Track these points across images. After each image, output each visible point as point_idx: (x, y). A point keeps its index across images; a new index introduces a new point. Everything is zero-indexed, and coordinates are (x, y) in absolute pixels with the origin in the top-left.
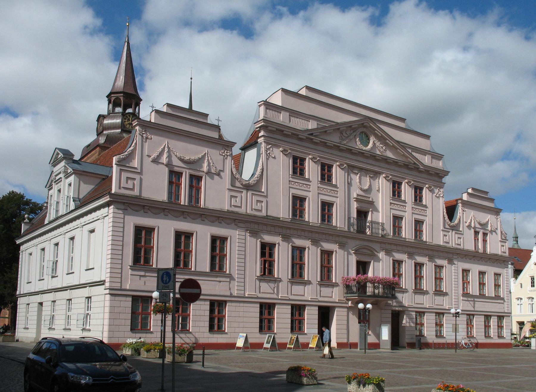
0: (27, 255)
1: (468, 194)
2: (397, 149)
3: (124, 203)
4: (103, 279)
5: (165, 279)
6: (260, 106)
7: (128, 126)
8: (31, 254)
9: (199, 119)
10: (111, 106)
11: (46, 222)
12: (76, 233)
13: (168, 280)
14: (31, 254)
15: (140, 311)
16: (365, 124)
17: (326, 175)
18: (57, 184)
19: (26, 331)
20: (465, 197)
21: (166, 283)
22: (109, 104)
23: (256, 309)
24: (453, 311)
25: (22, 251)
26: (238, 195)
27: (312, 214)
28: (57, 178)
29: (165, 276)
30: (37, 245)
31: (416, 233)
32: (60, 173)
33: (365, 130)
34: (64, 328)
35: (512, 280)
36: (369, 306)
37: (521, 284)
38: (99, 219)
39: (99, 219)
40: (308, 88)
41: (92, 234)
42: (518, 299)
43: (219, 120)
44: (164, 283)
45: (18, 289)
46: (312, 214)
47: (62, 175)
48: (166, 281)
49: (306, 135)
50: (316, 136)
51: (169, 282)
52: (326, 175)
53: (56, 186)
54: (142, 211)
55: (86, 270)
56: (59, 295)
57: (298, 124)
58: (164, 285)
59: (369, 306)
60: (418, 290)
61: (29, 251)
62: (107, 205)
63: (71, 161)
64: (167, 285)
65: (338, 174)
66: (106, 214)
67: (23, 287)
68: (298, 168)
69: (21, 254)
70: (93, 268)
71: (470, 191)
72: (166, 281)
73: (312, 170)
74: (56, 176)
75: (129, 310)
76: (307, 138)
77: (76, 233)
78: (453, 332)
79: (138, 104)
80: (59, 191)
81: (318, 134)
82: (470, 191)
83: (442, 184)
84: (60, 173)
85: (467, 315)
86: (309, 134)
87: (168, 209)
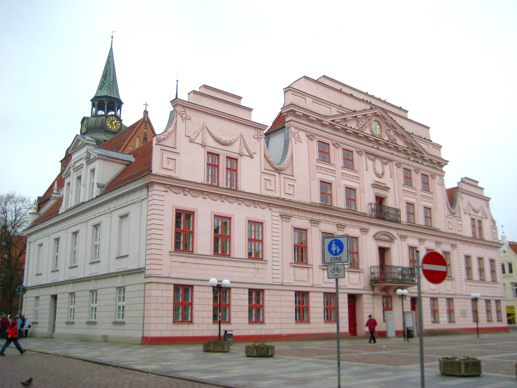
0: (37, 247)
2: (405, 137)
3: (165, 184)
4: (142, 266)
5: (333, 249)
8: (41, 245)
9: (233, 100)
10: (94, 109)
13: (338, 250)
14: (41, 245)
15: (181, 301)
16: (378, 113)
17: (348, 162)
18: (76, 171)
21: (336, 254)
22: (92, 108)
23: (292, 297)
25: (30, 243)
26: (272, 178)
27: (339, 200)
28: (77, 165)
29: (333, 245)
30: (49, 236)
34: (87, 321)
38: (135, 203)
41: (125, 221)
44: (333, 254)
46: (339, 200)
47: (83, 162)
48: (336, 251)
49: (329, 120)
50: (337, 122)
51: (341, 252)
52: (348, 162)
53: (75, 173)
54: (182, 194)
55: (70, 268)
57: (323, 110)
58: (333, 256)
61: (39, 242)
64: (337, 256)
65: (360, 161)
66: (145, 197)
67: (30, 279)
68: (324, 154)
69: (28, 245)
70: (127, 256)
72: (336, 251)
73: (337, 155)
74: (75, 163)
75: (171, 300)
76: (330, 124)
77: (105, 221)
79: (120, 107)
80: (79, 178)
81: (339, 120)
84: (81, 159)
86: (331, 121)
87: (208, 190)
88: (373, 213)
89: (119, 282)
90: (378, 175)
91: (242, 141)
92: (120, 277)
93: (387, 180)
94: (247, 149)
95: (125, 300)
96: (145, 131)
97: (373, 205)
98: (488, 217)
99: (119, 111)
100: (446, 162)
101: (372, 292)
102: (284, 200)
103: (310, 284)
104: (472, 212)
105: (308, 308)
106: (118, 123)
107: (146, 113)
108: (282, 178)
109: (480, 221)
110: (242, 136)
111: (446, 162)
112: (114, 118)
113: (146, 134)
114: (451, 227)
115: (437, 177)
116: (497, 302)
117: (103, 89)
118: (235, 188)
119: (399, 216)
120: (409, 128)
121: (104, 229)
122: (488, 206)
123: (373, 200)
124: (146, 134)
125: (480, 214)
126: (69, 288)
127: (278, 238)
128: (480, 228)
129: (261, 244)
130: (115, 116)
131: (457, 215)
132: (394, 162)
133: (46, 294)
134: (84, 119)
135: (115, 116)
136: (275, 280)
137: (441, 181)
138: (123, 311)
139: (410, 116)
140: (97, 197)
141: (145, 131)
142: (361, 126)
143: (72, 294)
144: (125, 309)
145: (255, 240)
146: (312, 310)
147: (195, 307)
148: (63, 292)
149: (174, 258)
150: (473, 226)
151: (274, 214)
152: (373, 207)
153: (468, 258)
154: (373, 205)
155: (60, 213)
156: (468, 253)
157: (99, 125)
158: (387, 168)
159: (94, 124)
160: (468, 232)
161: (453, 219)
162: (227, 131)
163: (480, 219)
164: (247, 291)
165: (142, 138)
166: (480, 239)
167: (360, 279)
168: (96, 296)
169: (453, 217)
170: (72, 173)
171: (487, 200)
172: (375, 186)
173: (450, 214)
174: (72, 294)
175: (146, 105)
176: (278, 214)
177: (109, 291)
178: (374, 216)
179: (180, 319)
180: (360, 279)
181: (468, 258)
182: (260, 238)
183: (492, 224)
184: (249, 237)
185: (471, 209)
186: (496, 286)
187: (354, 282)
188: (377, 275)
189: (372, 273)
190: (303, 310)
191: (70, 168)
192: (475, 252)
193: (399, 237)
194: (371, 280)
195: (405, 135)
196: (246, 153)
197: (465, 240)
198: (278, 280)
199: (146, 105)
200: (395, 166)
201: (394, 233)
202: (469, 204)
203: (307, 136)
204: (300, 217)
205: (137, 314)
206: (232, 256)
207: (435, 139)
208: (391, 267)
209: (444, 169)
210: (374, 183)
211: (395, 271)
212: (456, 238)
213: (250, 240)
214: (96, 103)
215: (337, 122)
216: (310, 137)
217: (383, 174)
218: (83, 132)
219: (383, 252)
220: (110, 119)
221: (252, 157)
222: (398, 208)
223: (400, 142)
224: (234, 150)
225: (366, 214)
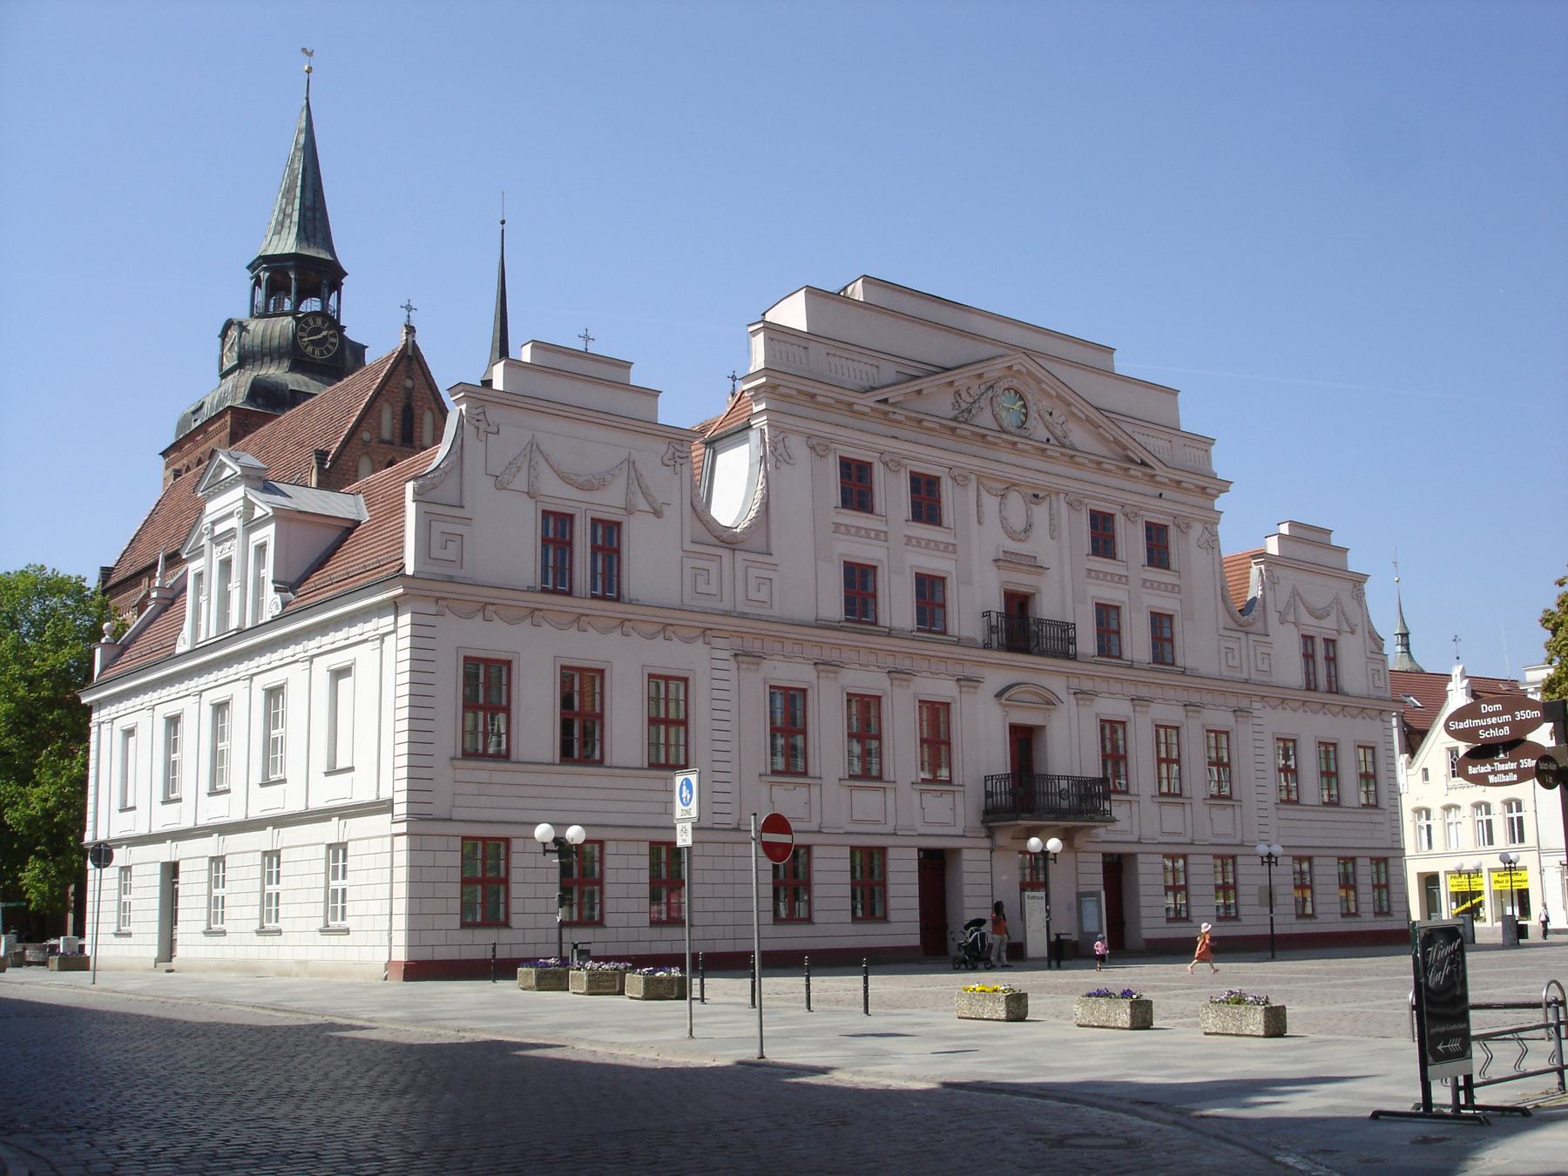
1: (1281, 537)
6: (754, 333)
7: (310, 348)
8: (129, 733)
10: (260, 295)
11: (181, 648)
12: (295, 678)
19: (123, 940)
20: (1273, 547)
24: (1262, 849)
26: (713, 566)
28: (219, 529)
31: (1154, 646)
32: (230, 515)
33: (1015, 383)
35: (1401, 759)
36: (1054, 844)
37: (1425, 770)
38: (366, 641)
39: (366, 641)
40: (867, 280)
41: (344, 684)
42: (1418, 811)
43: (587, 338)
45: (89, 826)
47: (235, 522)
56: (235, 841)
59: (1054, 844)
60: (1172, 796)
62: (395, 607)
63: (261, 485)
66: (391, 628)
69: (94, 730)
71: (1284, 529)
74: (214, 523)
78: (1261, 905)
79: (336, 286)
82: (1284, 529)
83: (1211, 515)
84: (230, 515)
85: (1216, 857)
88: (994, 637)
89: (330, 831)
90: (1012, 534)
91: (633, 475)
92: (335, 819)
93: (1040, 545)
94: (646, 495)
95: (348, 874)
96: (409, 383)
97: (994, 615)
98: (1359, 630)
99: (334, 295)
100: (1224, 486)
101: (987, 843)
102: (743, 616)
103: (814, 826)
104: (1306, 618)
105: (883, 885)
106: (333, 336)
107: (411, 330)
108: (740, 565)
109: (1330, 643)
110: (631, 463)
111: (1224, 486)
112: (319, 321)
113: (409, 393)
114: (1235, 663)
115: (1197, 529)
116: (1227, 860)
117: (285, 231)
118: (614, 595)
119: (1073, 641)
120: (1111, 397)
121: (294, 702)
122: (1359, 596)
123: (997, 604)
124: (409, 393)
125: (1330, 623)
126: (211, 845)
127: (728, 710)
128: (1331, 660)
129: (682, 729)
130: (323, 314)
131: (1259, 626)
132: (1062, 496)
133: (146, 863)
134: (229, 325)
135: (323, 314)
136: (718, 818)
137: (1207, 535)
138: (343, 901)
139: (1121, 366)
140: (275, 619)
141: (409, 383)
142: (964, 406)
143: (218, 861)
144: (348, 898)
145: (668, 722)
146: (892, 890)
147: (515, 890)
148: (193, 856)
149: (1283, 814)
150: (1309, 657)
151: (718, 654)
152: (994, 622)
153: (1288, 746)
154: (994, 615)
155: (179, 651)
156: (1288, 730)
157: (275, 342)
158: (1040, 513)
159: (258, 341)
160: (1291, 671)
161: (1243, 642)
162: (597, 450)
163: (1332, 635)
164: (645, 848)
165: (400, 406)
166: (1330, 691)
167: (954, 809)
168: (345, 859)
169: (1242, 635)
170: (207, 549)
171: (1359, 580)
172: (1005, 560)
173: (1235, 626)
174: (218, 861)
175: (409, 308)
176: (726, 655)
177: (309, 853)
178: (995, 644)
179: (479, 918)
180: (954, 809)
181: (1288, 746)
182: (682, 716)
183: (1371, 645)
184: (653, 715)
185: (1303, 610)
186: (1376, 818)
187: (947, 816)
188: (1003, 800)
189: (988, 795)
190: (872, 891)
191: (201, 535)
192: (1310, 727)
193: (1072, 698)
194: (987, 812)
195: (1102, 418)
196: (642, 504)
197: (1280, 698)
198: (727, 819)
199: (409, 308)
200: (1064, 507)
201: (1057, 685)
202: (1295, 593)
203: (813, 448)
204: (788, 658)
205: (375, 907)
206: (607, 762)
207: (1189, 422)
208: (1047, 778)
209: (1219, 504)
210: (1001, 556)
211: (1052, 788)
212: (1250, 693)
213: (653, 721)
214: (264, 276)
215: (893, 404)
216: (818, 448)
217: (1028, 528)
218: (227, 365)
219: (1024, 740)
220: (307, 323)
221: (657, 513)
222: (1070, 620)
223: (1079, 437)
224: (609, 502)
225: (973, 640)
